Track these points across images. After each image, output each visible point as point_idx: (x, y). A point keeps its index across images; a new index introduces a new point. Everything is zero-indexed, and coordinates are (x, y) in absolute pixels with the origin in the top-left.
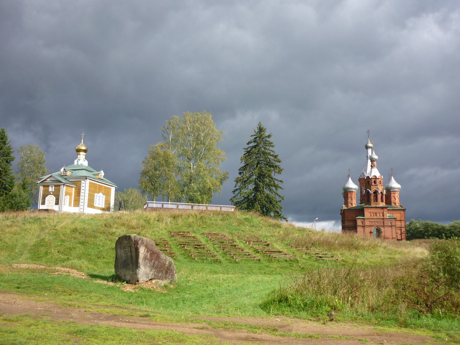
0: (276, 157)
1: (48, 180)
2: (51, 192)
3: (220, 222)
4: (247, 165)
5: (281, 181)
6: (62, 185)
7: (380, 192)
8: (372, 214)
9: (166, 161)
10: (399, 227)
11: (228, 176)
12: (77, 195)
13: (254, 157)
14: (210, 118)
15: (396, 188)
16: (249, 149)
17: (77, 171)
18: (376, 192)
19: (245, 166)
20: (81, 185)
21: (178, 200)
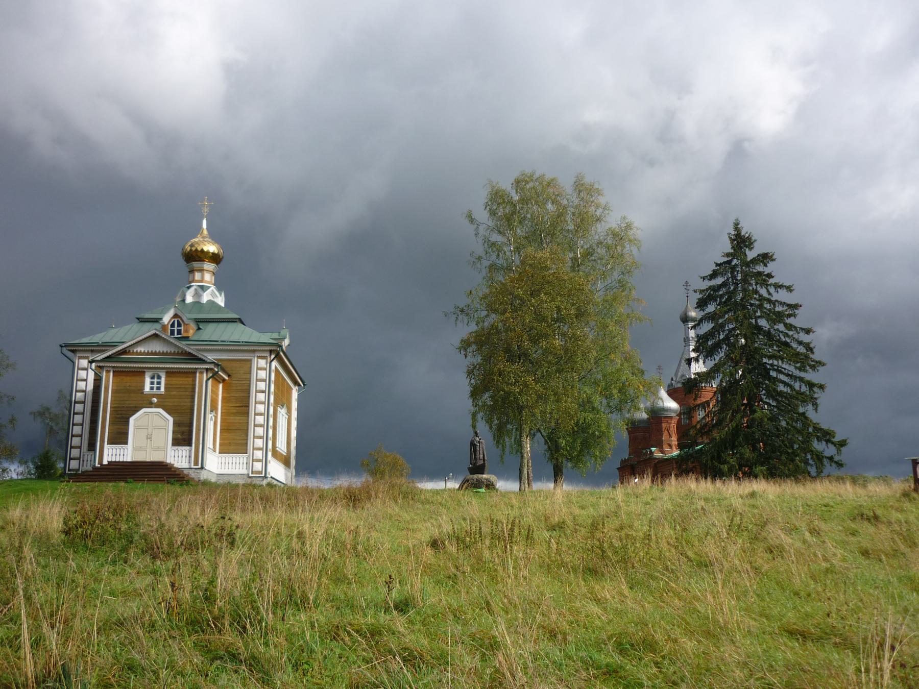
1: (140, 349)
2: (154, 396)
6: (201, 373)
10: (268, 470)
12: (234, 410)
17: (222, 326)
20: (250, 373)
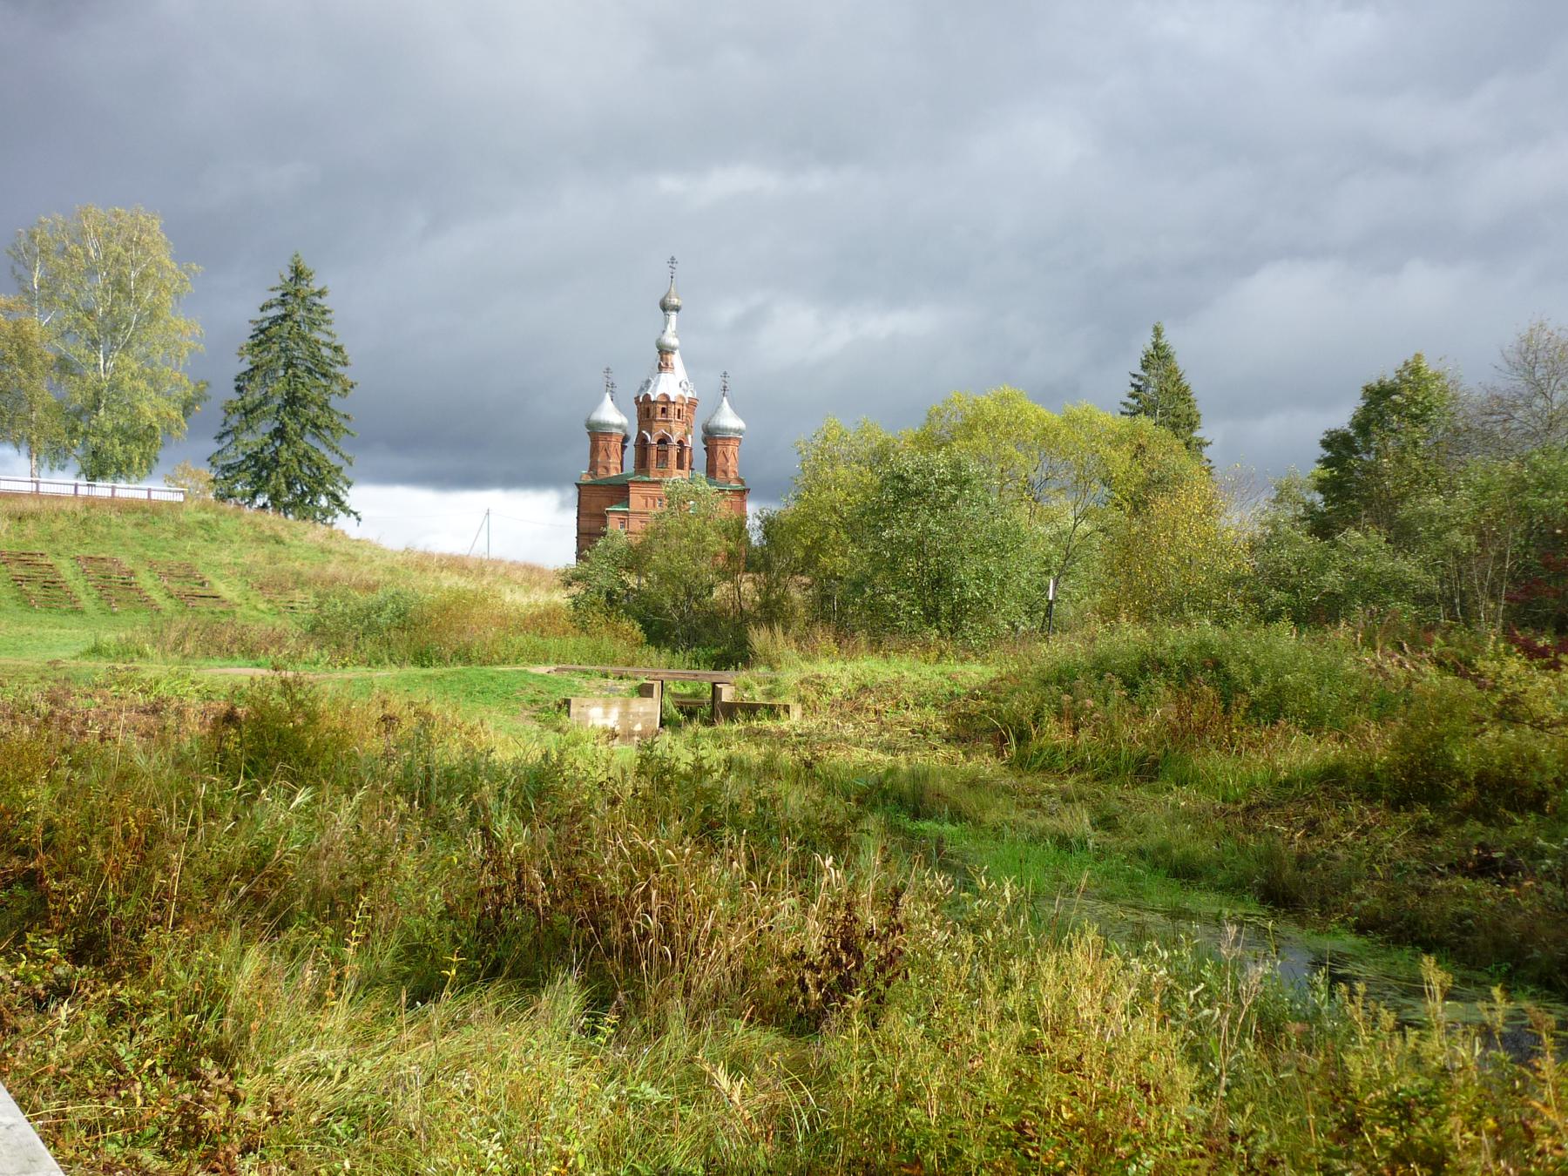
0: (337, 349)
3: (130, 531)
4: (257, 367)
5: (346, 417)
7: (674, 440)
8: (650, 501)
9: (21, 352)
11: (207, 391)
13: (276, 348)
14: (157, 227)
15: (731, 430)
16: (266, 324)
18: (663, 441)
19: (252, 370)
21: (56, 455)
